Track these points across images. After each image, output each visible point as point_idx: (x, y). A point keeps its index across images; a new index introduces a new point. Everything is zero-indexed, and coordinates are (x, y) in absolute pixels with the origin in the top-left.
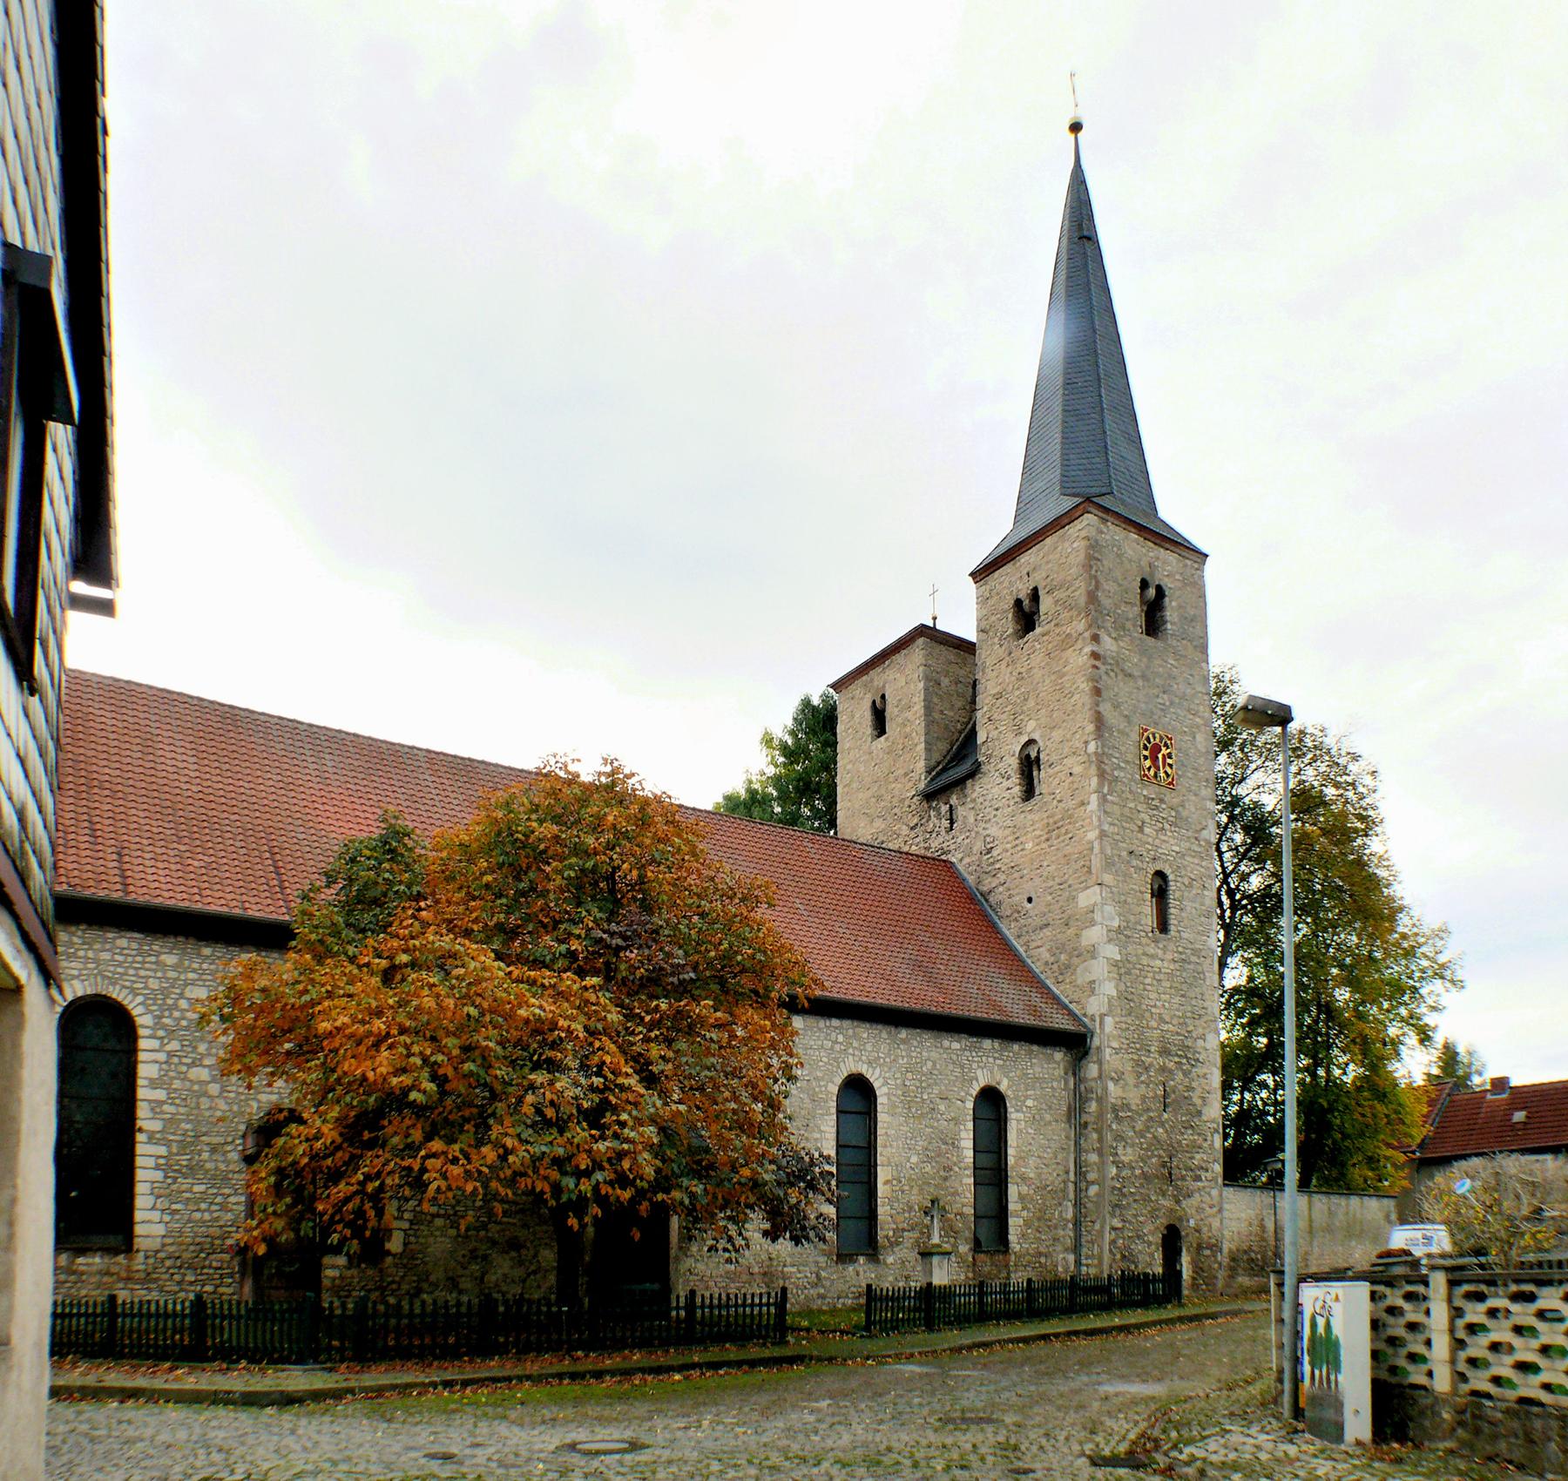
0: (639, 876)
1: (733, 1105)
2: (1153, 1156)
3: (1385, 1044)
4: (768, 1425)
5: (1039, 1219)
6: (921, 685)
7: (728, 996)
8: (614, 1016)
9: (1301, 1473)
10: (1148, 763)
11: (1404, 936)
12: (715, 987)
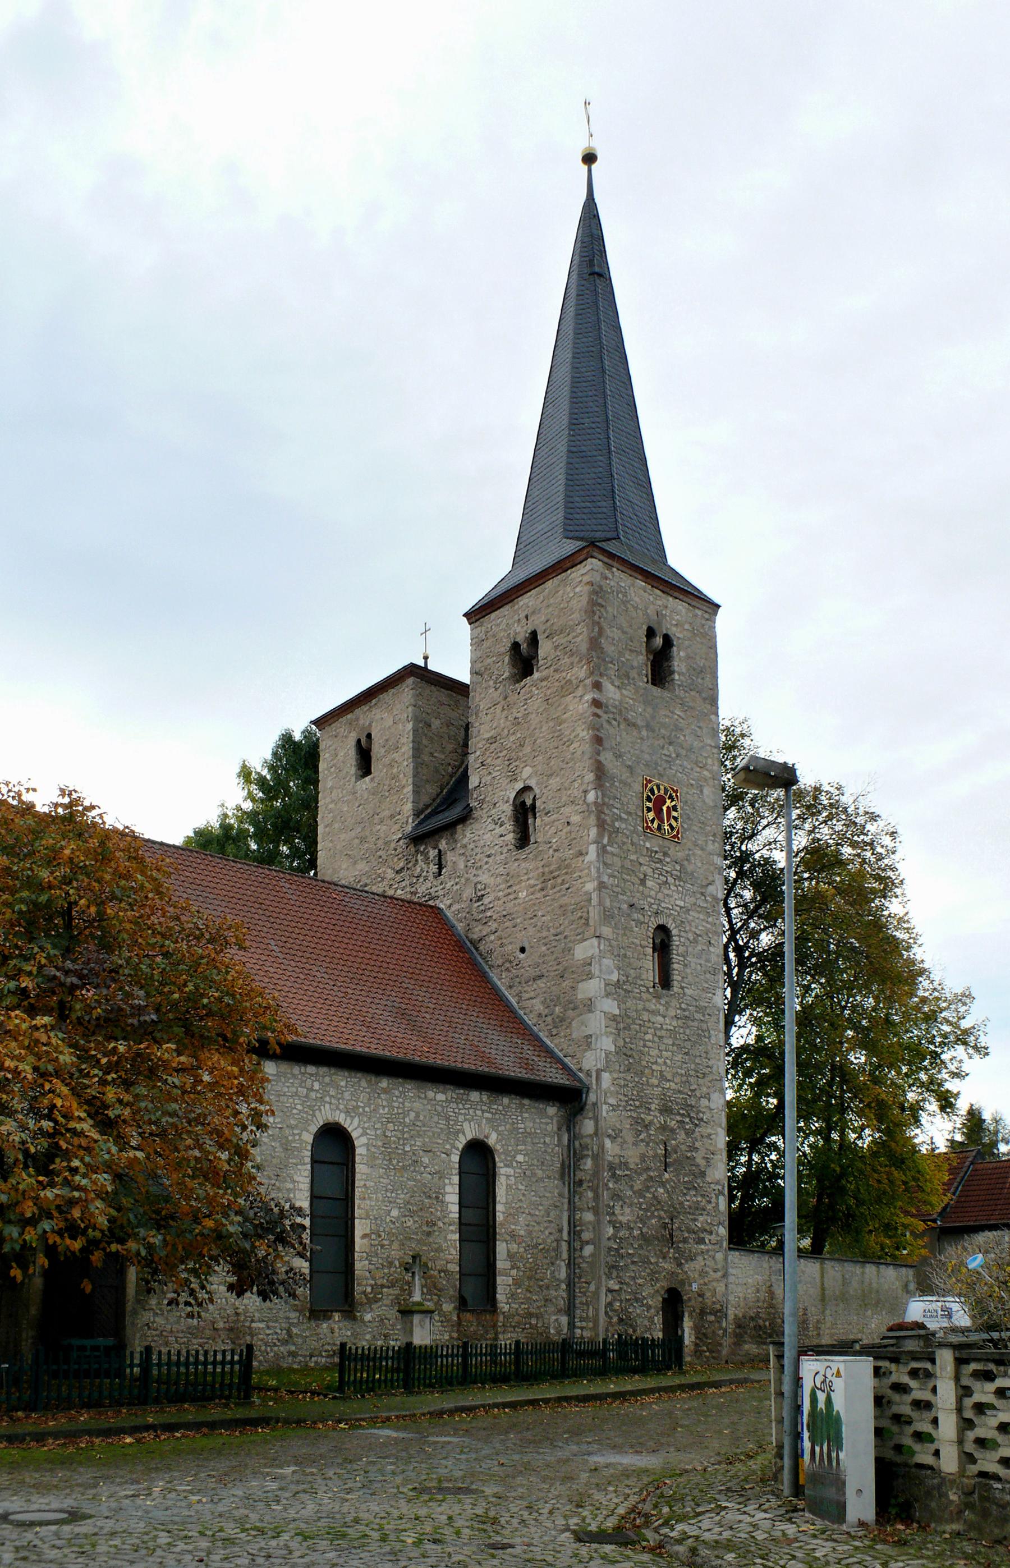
0: (98, 913)
1: (197, 1153)
2: (653, 1216)
3: (903, 1109)
4: (224, 1493)
5: (530, 1278)
6: (410, 726)
7: (193, 1040)
8: (67, 1057)
9: (799, 1554)
10: (651, 815)
11: (924, 1000)
12: (179, 1030)
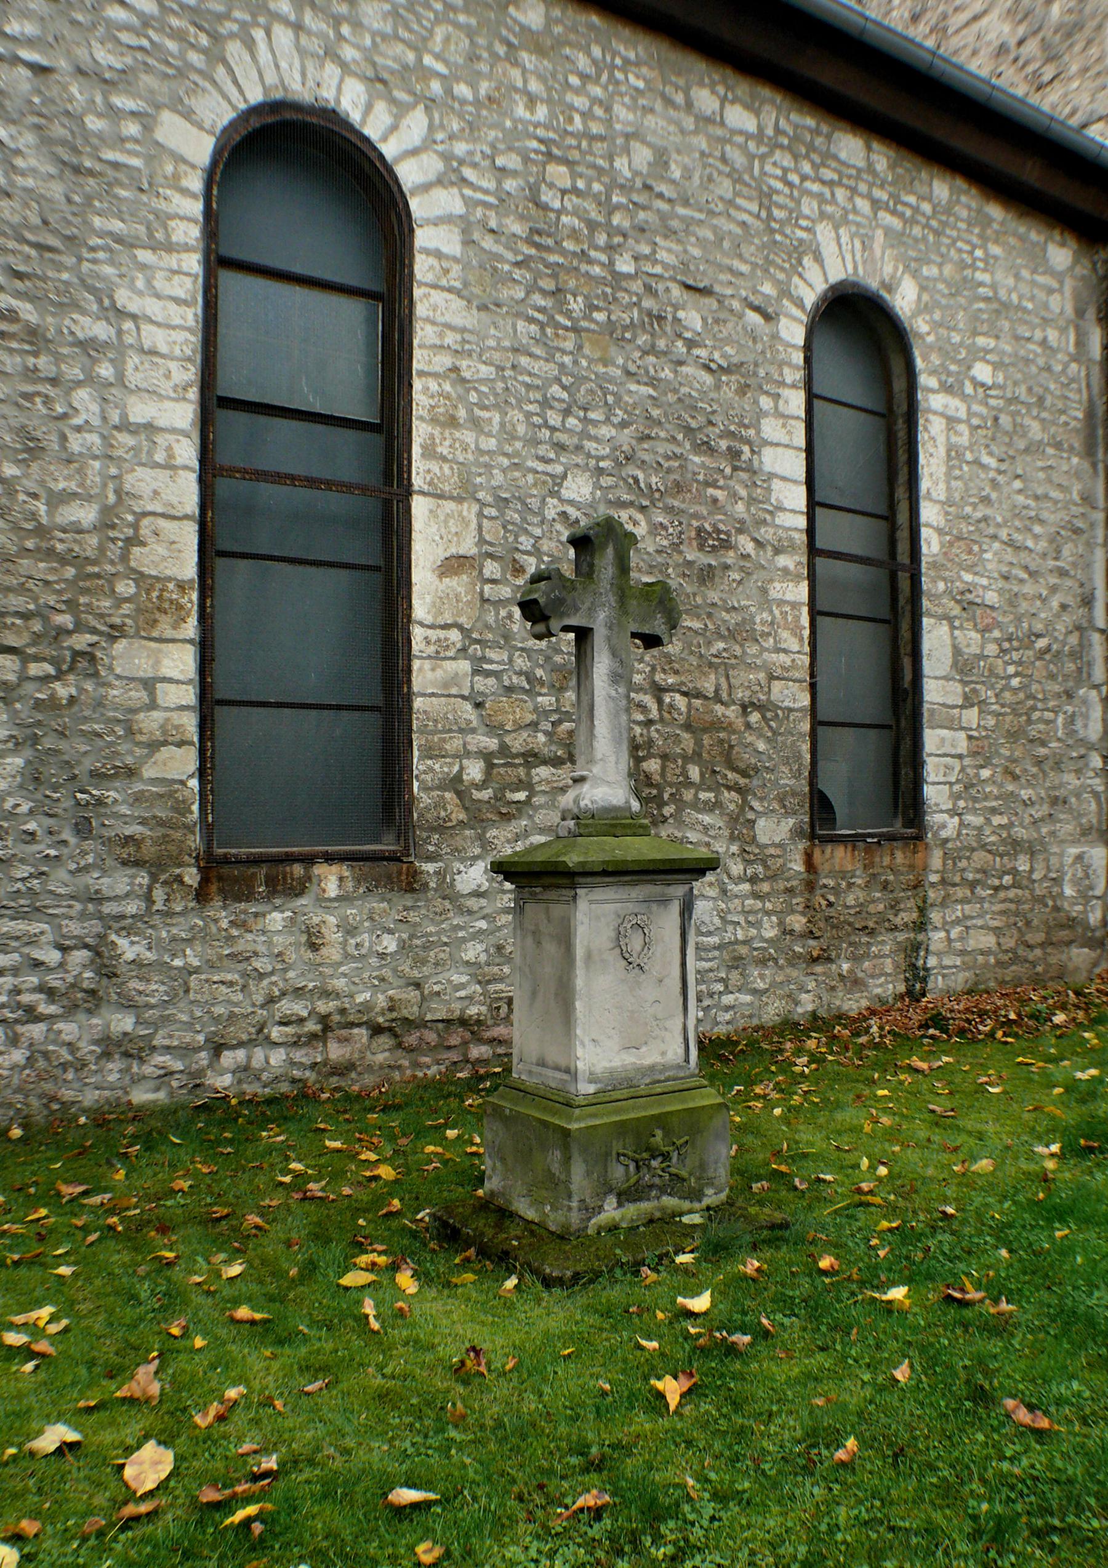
5: (1013, 736)
